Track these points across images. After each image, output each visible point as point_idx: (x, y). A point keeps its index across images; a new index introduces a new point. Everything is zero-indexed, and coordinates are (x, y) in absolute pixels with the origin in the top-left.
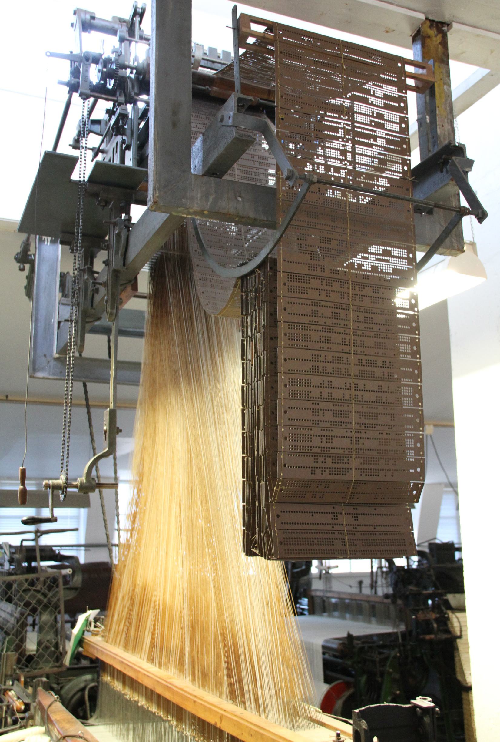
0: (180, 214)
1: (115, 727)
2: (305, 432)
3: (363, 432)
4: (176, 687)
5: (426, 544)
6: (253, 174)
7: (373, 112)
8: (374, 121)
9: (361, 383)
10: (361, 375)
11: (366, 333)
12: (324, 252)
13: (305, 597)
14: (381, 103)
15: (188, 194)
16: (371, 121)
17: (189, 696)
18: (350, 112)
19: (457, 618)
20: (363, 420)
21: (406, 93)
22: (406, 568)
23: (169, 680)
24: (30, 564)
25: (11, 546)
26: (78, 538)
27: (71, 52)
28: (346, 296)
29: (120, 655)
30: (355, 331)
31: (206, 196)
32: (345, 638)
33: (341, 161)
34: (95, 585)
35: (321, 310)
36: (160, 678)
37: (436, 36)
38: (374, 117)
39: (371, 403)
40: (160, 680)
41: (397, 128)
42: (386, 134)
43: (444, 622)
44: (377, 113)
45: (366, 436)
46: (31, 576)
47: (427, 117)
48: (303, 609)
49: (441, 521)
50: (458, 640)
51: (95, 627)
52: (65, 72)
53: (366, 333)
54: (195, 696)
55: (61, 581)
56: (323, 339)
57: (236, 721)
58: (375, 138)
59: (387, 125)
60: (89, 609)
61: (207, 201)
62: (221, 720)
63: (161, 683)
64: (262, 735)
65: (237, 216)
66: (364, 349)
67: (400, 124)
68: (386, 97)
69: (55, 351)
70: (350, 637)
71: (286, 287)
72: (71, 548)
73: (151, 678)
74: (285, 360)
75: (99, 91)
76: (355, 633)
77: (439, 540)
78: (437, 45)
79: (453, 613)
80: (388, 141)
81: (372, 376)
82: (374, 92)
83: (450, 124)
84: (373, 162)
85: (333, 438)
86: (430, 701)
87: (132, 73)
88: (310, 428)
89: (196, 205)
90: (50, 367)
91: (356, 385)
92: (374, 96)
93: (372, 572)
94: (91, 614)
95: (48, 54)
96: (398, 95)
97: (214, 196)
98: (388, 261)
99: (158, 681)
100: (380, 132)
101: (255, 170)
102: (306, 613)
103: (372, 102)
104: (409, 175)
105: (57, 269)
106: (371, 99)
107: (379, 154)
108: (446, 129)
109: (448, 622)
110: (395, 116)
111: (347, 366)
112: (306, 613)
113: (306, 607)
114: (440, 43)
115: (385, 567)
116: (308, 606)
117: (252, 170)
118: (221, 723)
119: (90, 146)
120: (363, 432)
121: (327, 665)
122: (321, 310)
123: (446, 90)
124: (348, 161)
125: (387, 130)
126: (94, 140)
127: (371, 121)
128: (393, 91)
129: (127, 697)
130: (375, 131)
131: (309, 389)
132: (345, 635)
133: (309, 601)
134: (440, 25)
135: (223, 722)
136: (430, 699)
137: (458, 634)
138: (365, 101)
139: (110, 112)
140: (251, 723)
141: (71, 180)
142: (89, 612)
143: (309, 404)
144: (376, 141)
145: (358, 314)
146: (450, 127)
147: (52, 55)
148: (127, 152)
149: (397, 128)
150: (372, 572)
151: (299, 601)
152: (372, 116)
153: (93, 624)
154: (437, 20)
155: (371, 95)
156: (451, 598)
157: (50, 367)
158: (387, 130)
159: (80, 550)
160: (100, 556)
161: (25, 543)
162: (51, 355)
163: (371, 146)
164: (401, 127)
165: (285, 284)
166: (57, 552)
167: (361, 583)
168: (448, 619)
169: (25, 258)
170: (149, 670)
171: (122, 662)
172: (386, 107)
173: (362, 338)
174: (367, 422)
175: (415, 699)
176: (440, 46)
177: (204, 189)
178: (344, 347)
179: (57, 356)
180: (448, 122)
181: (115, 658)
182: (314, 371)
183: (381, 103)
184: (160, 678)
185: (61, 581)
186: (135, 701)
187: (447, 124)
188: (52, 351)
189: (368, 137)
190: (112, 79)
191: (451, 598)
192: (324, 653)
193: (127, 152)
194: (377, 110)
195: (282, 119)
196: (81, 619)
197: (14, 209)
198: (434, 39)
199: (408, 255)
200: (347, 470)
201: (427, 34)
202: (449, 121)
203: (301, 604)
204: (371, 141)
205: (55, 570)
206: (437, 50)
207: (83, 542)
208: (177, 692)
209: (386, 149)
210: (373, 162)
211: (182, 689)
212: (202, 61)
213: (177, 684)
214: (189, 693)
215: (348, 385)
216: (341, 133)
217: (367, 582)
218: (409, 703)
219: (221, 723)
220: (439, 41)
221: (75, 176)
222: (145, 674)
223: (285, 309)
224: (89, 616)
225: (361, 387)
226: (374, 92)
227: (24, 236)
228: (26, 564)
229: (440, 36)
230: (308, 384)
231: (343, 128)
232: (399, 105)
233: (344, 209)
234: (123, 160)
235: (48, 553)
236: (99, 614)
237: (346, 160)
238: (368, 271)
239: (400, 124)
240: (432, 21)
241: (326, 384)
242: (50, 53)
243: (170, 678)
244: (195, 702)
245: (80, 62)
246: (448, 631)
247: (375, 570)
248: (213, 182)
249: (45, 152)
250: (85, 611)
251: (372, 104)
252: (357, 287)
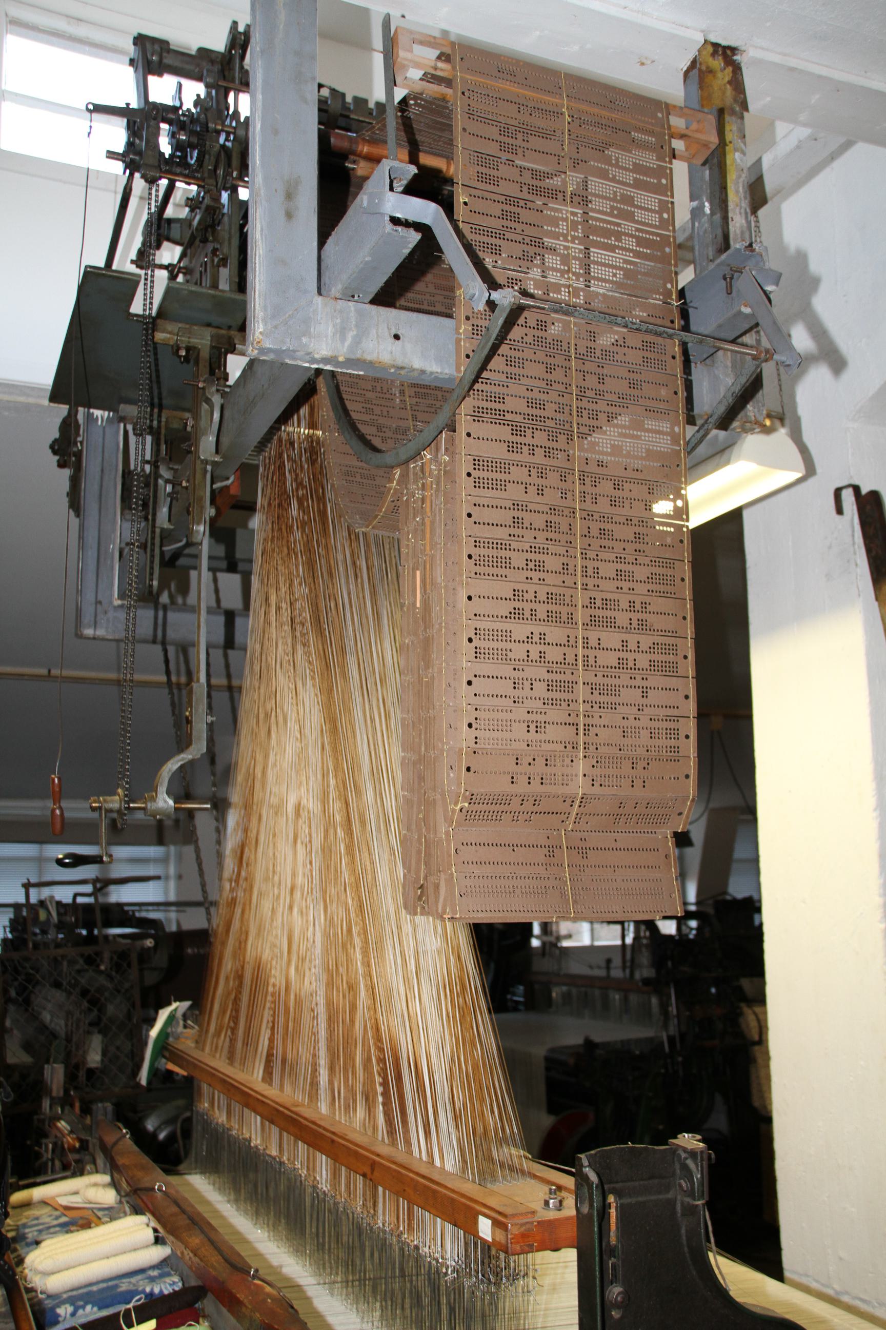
0: (300, 363)
1: (212, 1178)
2: (500, 716)
3: (596, 715)
4: (305, 1119)
5: (710, 902)
6: (425, 303)
7: (615, 193)
8: (617, 208)
9: (593, 636)
10: (593, 622)
11: (602, 555)
12: (534, 422)
13: (521, 984)
14: (630, 177)
15: (312, 330)
16: (612, 208)
17: (324, 1132)
18: (582, 199)
19: (756, 1014)
20: (596, 697)
21: (671, 163)
22: (677, 938)
23: (294, 1109)
24: (90, 932)
25: (59, 904)
26: (166, 892)
27: (128, 104)
28: (569, 495)
29: (222, 1070)
30: (584, 552)
31: (342, 332)
32: (579, 1046)
33: (563, 273)
34: (182, 961)
35: (527, 518)
36: (281, 1106)
37: (723, 70)
38: (617, 202)
39: (609, 669)
40: (281, 1109)
41: (654, 219)
42: (637, 230)
43: (734, 1018)
44: (622, 195)
45: (602, 722)
46: (89, 950)
47: (707, 204)
48: (517, 1002)
49: (735, 866)
50: (756, 1048)
51: (185, 1027)
52: (116, 135)
53: (602, 555)
54: (334, 1133)
55: (134, 957)
56: (531, 565)
57: (395, 1170)
58: (618, 235)
59: (639, 215)
60: (175, 1001)
61: (343, 339)
62: (373, 1170)
63: (283, 1113)
64: (435, 1192)
65: (393, 366)
66: (599, 582)
67: (660, 213)
68: (638, 168)
69: (116, 596)
70: (589, 1044)
71: (471, 479)
72: (155, 908)
73: (268, 1104)
74: (470, 598)
75: (174, 167)
76: (597, 1038)
77: (730, 895)
78: (725, 85)
79: (749, 1006)
80: (640, 242)
81: (611, 624)
82: (617, 159)
83: (743, 215)
84: (615, 275)
85: (547, 725)
86: (699, 1141)
87: (227, 140)
88: (509, 709)
89: (324, 347)
90: (108, 620)
91: (586, 639)
92: (617, 165)
93: (624, 945)
94: (178, 1007)
95: (91, 107)
96: (658, 165)
97: (355, 333)
98: (638, 437)
99: (278, 1110)
100: (628, 226)
101: (427, 297)
102: (521, 1007)
103: (614, 176)
104: (674, 297)
105: (117, 466)
106: (613, 171)
107: (625, 261)
108: (738, 225)
109: (741, 1020)
110: (650, 200)
111: (570, 609)
112: (521, 1007)
113: (521, 999)
114: (729, 82)
115: (645, 937)
116: (524, 997)
117: (423, 297)
118: (372, 1173)
119: (166, 262)
120: (596, 715)
121: (552, 1086)
122: (527, 518)
123: (738, 161)
124: (574, 274)
125: (637, 222)
126: (169, 254)
127: (612, 208)
128: (650, 160)
129: (234, 1132)
130: (619, 225)
131: (509, 646)
132: (580, 1041)
133: (525, 990)
134: (729, 52)
135: (376, 1173)
136: (699, 1137)
137: (756, 1038)
138: (604, 175)
139: (192, 203)
140: (418, 1174)
141: (130, 314)
142: (175, 1005)
143: (507, 670)
144: (620, 240)
145: (591, 524)
146: (744, 221)
147: (99, 109)
148: (221, 269)
149: (654, 219)
150: (624, 945)
151: (511, 989)
152: (614, 200)
153: (181, 1023)
154: (724, 43)
155: (611, 164)
156: (746, 984)
157: (108, 620)
158: (637, 222)
159: (169, 911)
160: (194, 921)
161: (80, 900)
162: (111, 602)
163: (612, 248)
164: (661, 218)
165: (469, 475)
166: (131, 913)
167: (609, 961)
168: (741, 1014)
169: (66, 448)
170: (265, 1093)
171: (224, 1081)
172: (638, 185)
173: (596, 564)
174: (602, 699)
175: (676, 1138)
176: (728, 86)
177: (338, 321)
178: (565, 578)
179: (119, 602)
180: (740, 213)
181: (214, 1075)
182: (516, 614)
183: (630, 177)
184: (281, 1106)
185: (134, 957)
186: (245, 1139)
187: (739, 216)
188: (112, 595)
189: (607, 233)
190: (194, 149)
191: (746, 984)
192: (547, 1069)
193: (221, 269)
194: (620, 190)
195: (465, 203)
196: (163, 1015)
197: (40, 363)
198: (720, 75)
199: (672, 429)
200: (569, 778)
201: (708, 67)
202: (743, 211)
203: (514, 994)
204: (612, 241)
205: (128, 941)
206: (724, 93)
207: (172, 898)
208: (307, 1126)
209: (637, 254)
210: (615, 275)
211: (314, 1123)
212: (340, 119)
213: (307, 1115)
214: (325, 1129)
215: (572, 640)
216: (563, 227)
217: (617, 961)
218: (667, 1144)
219: (372, 1173)
220: (727, 79)
221: (137, 307)
222: (258, 1099)
223: (469, 515)
224: (176, 1010)
225: (593, 642)
226: (617, 159)
227: (64, 409)
228: (84, 932)
229: (729, 69)
230: (507, 636)
231: (566, 220)
232: (660, 181)
233: (567, 353)
234: (215, 286)
235: (120, 914)
236: (190, 1008)
237: (568, 271)
238: (607, 454)
239: (660, 213)
240: (716, 45)
241: (536, 638)
242: (94, 105)
243: (298, 1106)
244: (333, 1141)
245: (142, 120)
246: (740, 1034)
247: (629, 940)
248: (352, 309)
249: (86, 267)
250: (169, 1004)
251: (614, 180)
252: (588, 481)
